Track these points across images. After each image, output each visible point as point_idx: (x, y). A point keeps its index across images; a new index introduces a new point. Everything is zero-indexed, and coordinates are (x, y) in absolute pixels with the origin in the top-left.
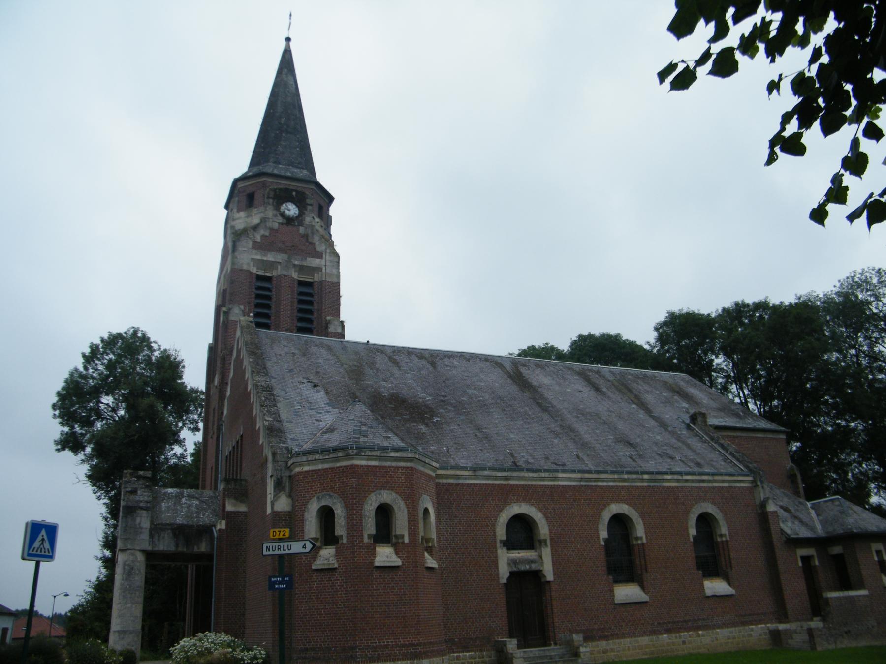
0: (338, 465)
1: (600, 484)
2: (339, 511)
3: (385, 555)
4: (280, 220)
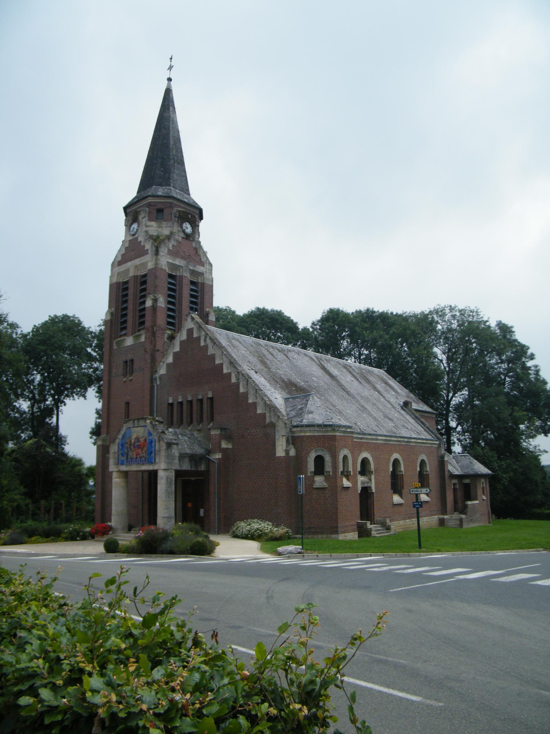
0: (327, 434)
1: (391, 443)
2: (328, 459)
3: (319, 481)
4: (182, 235)
